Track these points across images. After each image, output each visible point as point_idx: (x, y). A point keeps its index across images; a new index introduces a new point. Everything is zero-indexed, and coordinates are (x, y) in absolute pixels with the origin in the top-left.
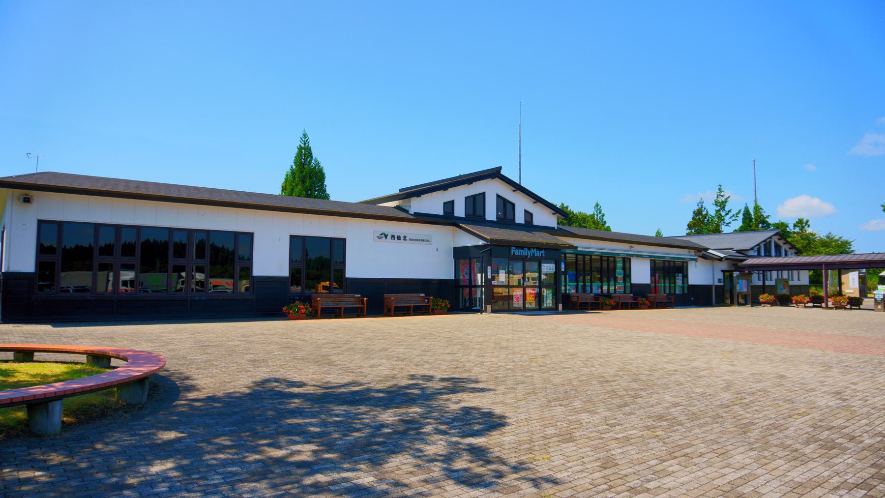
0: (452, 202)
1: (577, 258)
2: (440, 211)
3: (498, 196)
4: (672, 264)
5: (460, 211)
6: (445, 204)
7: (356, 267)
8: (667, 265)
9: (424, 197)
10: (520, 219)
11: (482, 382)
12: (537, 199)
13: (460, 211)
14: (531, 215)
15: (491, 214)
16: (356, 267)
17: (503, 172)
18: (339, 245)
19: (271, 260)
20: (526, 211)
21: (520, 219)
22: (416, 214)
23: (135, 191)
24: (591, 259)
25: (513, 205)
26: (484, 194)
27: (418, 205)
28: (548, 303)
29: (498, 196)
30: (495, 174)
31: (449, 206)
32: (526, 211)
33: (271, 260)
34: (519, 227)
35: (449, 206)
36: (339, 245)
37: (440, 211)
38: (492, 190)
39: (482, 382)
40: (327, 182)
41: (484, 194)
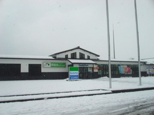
1: (103, 66)
2: (64, 57)
4: (135, 67)
5: (69, 56)
6: (65, 55)
7: (43, 70)
8: (133, 67)
12: (90, 53)
13: (69, 56)
14: (89, 56)
15: (78, 56)
16: (43, 70)
17: (80, 47)
18: (19, 65)
19: (25, 69)
20: (88, 56)
21: (86, 57)
22: (58, 58)
24: (106, 66)
25: (84, 54)
26: (76, 53)
27: (58, 56)
29: (80, 53)
30: (78, 48)
31: (67, 56)
32: (88, 56)
33: (25, 69)
36: (19, 65)
37: (64, 57)
38: (78, 52)
40: (145, 91)
41: (76, 53)
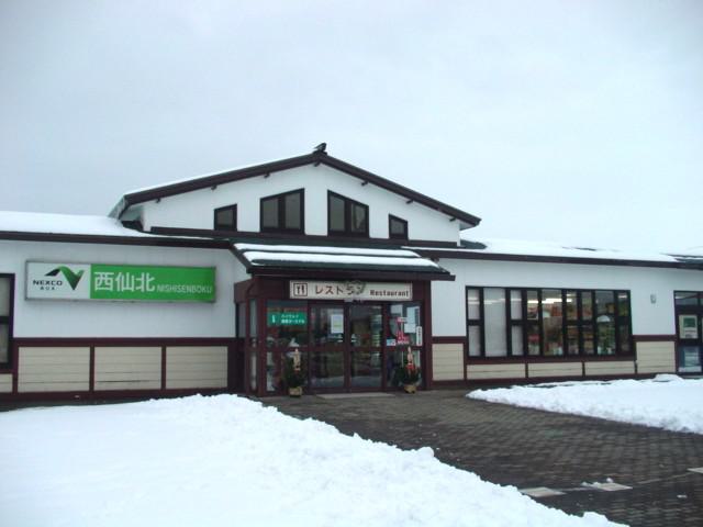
0: (233, 208)
3: (330, 194)
5: (249, 220)
9: (164, 200)
10: (379, 228)
11: (600, 250)
12: (412, 197)
13: (249, 220)
17: (331, 152)
20: (392, 218)
22: (155, 230)
23: (8, 295)
25: (366, 208)
26: (301, 192)
27: (155, 216)
28: (270, 386)
29: (330, 194)
31: (226, 215)
32: (392, 218)
34: (378, 244)
35: (226, 215)
38: (317, 188)
39: (600, 250)
41: (301, 192)
